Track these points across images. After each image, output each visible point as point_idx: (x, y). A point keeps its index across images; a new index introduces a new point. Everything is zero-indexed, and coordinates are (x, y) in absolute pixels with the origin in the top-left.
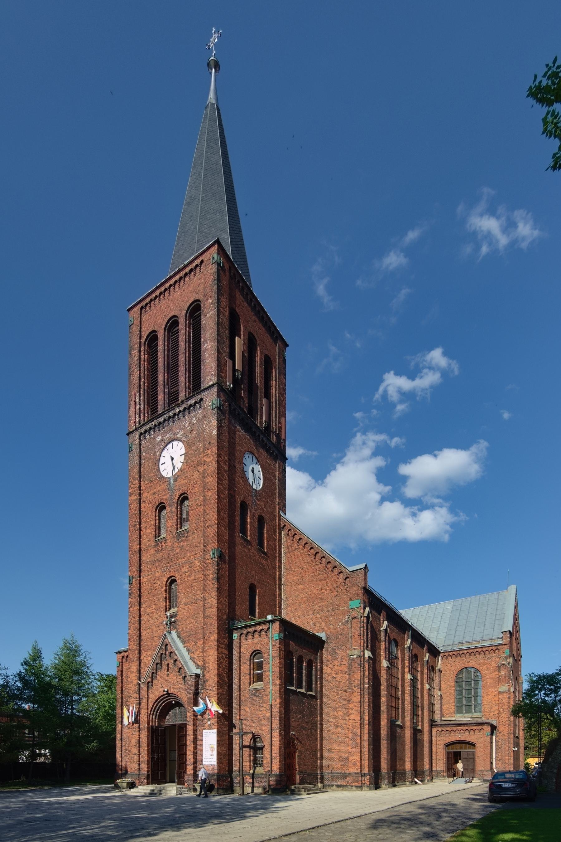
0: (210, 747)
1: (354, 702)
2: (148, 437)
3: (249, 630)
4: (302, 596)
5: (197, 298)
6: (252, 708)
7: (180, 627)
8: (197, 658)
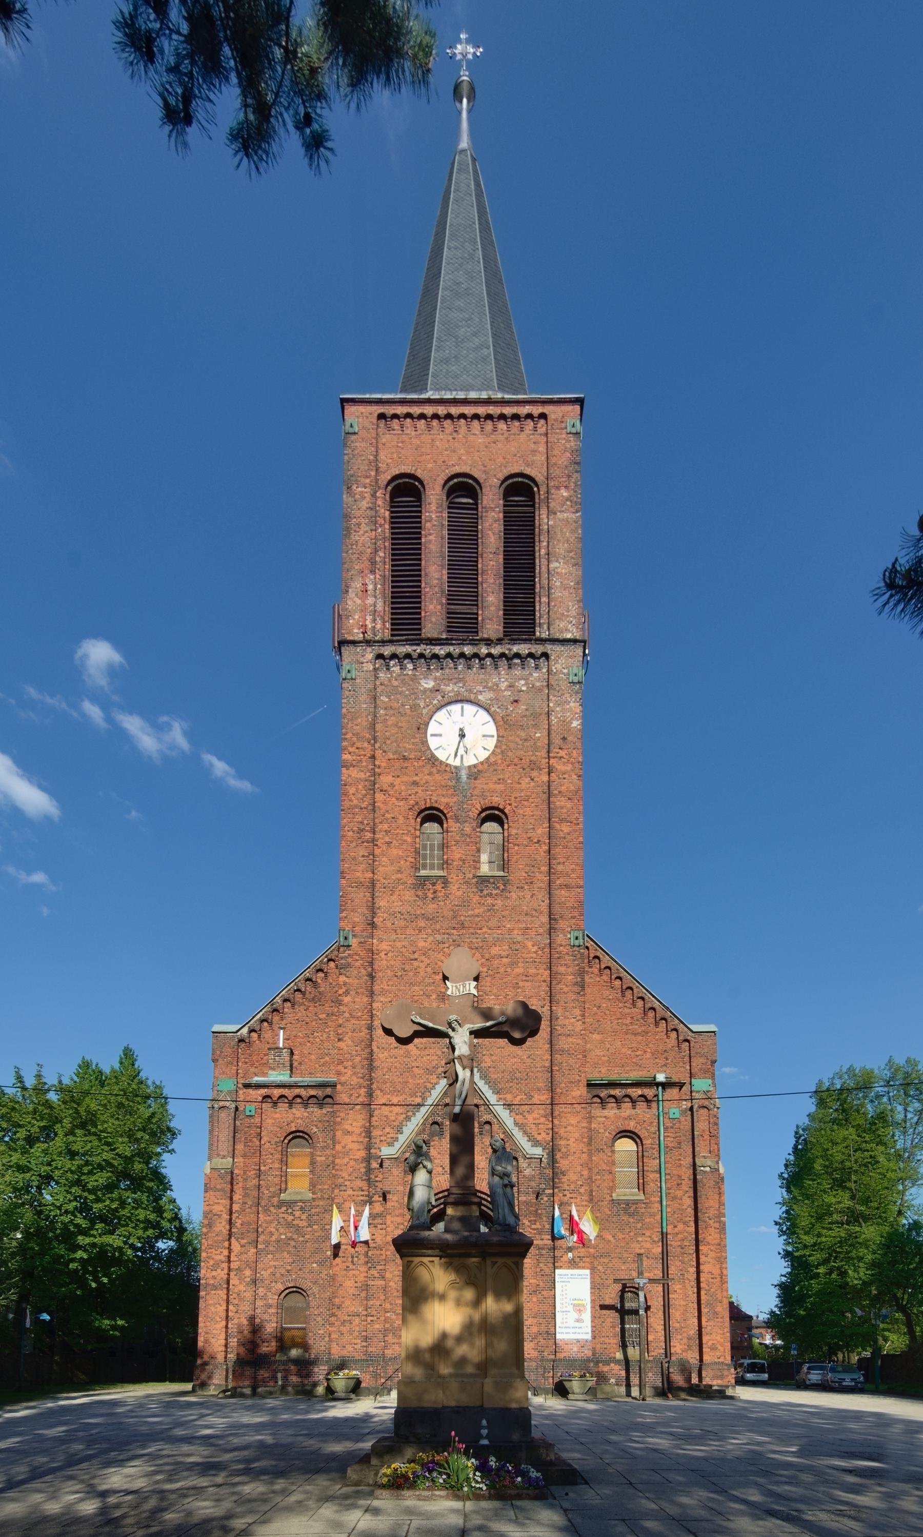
0: (574, 1305)
1: (709, 1244)
2: (397, 669)
3: (613, 1092)
4: (598, 1052)
6: (621, 1236)
7: (487, 1059)
8: (533, 1126)
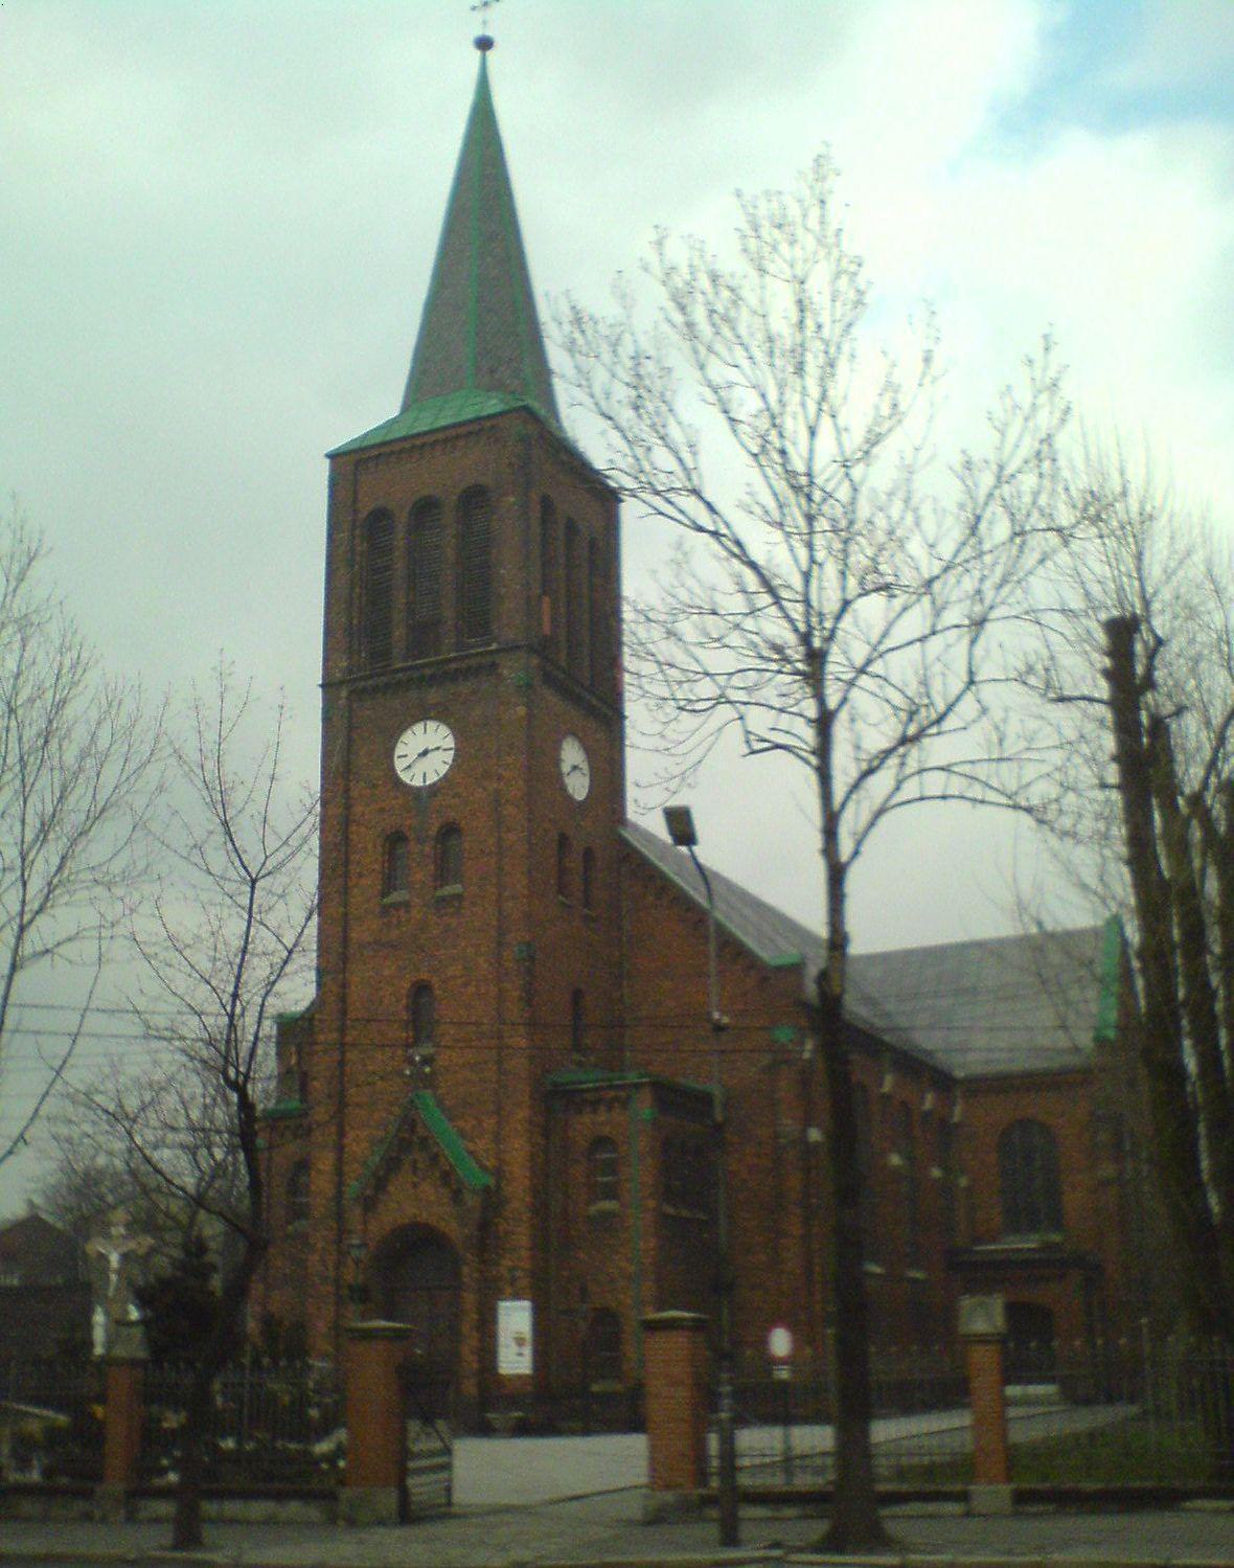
5: (483, 480)
